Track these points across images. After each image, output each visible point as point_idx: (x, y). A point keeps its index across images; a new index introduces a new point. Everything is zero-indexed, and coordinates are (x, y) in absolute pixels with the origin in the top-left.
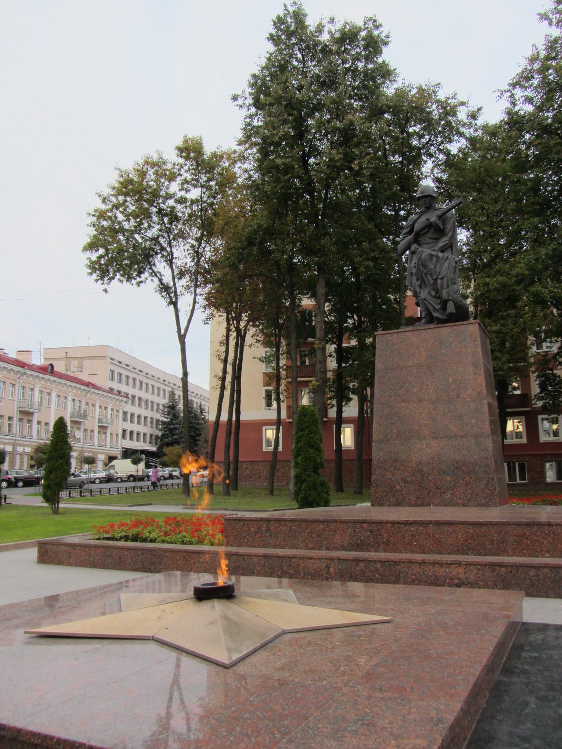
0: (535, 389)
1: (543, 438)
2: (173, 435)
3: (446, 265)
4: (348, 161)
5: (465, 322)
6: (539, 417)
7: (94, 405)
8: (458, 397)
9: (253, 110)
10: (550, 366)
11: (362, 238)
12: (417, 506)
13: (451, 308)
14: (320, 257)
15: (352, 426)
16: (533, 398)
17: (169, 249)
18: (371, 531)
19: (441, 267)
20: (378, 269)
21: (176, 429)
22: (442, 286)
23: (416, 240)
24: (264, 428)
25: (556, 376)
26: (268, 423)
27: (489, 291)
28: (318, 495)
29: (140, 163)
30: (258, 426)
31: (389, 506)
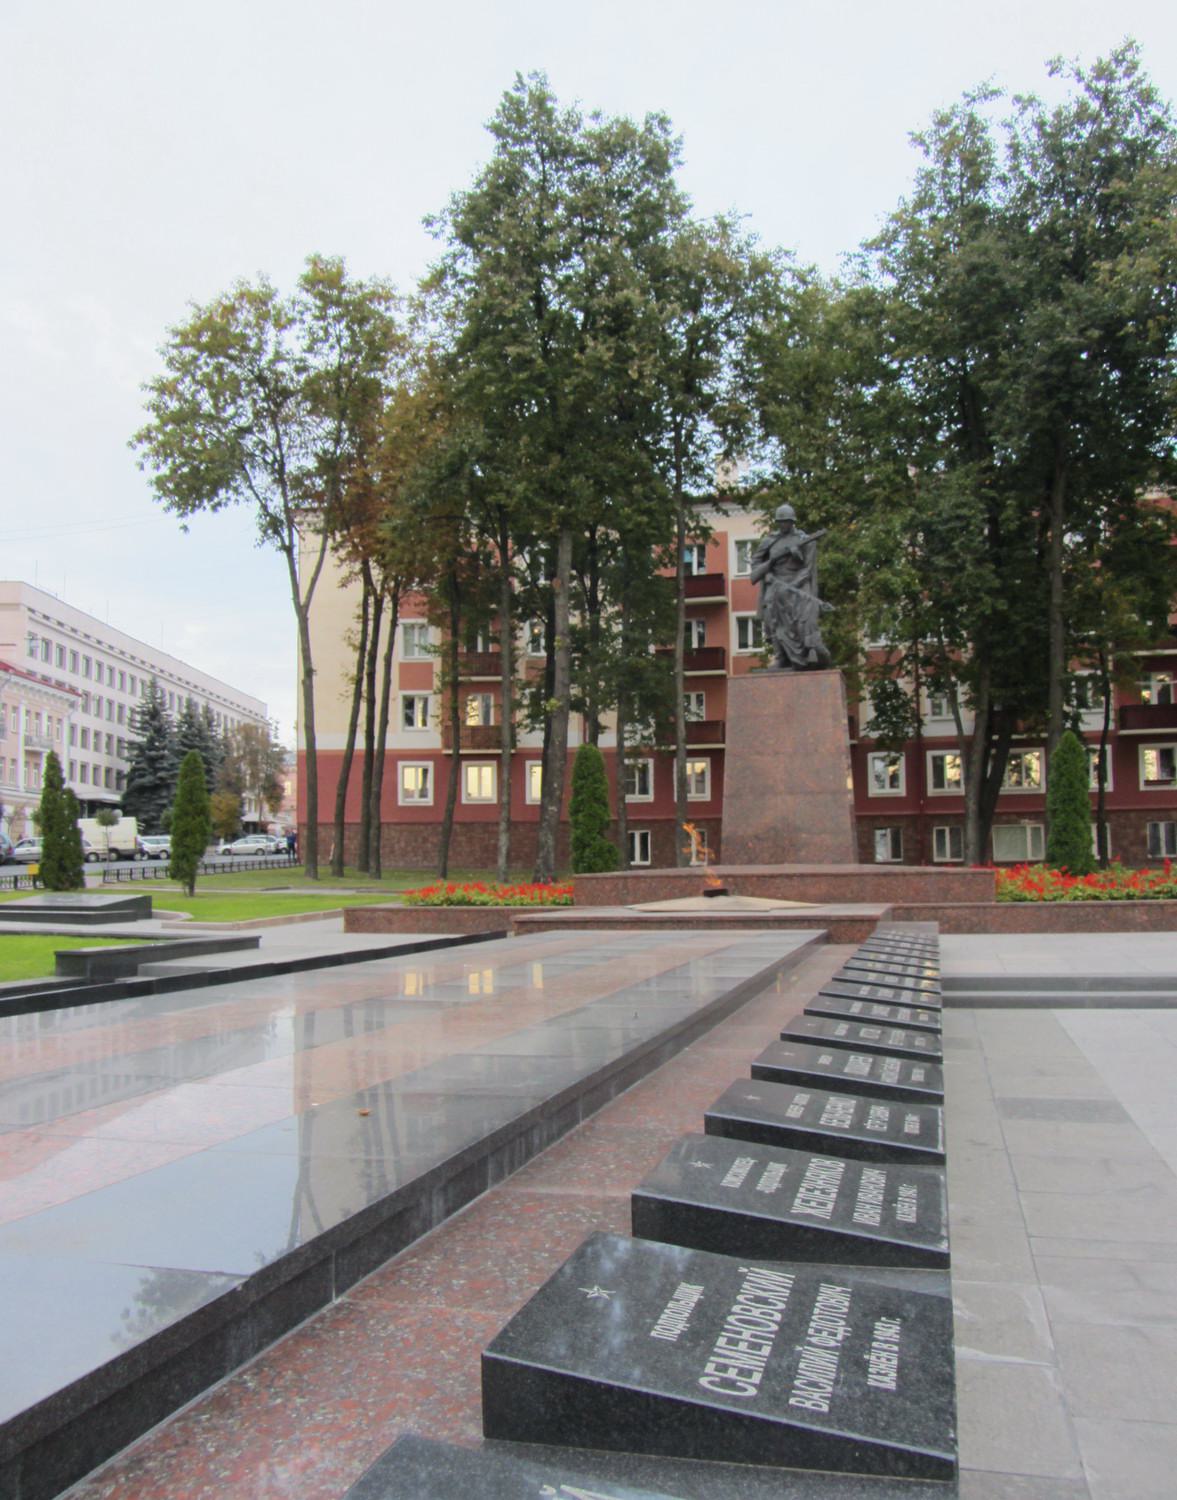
2: (157, 770)
3: (808, 607)
6: (870, 755)
7: (15, 709)
9: (457, 246)
14: (569, 506)
21: (163, 757)
23: (772, 569)
24: (401, 764)
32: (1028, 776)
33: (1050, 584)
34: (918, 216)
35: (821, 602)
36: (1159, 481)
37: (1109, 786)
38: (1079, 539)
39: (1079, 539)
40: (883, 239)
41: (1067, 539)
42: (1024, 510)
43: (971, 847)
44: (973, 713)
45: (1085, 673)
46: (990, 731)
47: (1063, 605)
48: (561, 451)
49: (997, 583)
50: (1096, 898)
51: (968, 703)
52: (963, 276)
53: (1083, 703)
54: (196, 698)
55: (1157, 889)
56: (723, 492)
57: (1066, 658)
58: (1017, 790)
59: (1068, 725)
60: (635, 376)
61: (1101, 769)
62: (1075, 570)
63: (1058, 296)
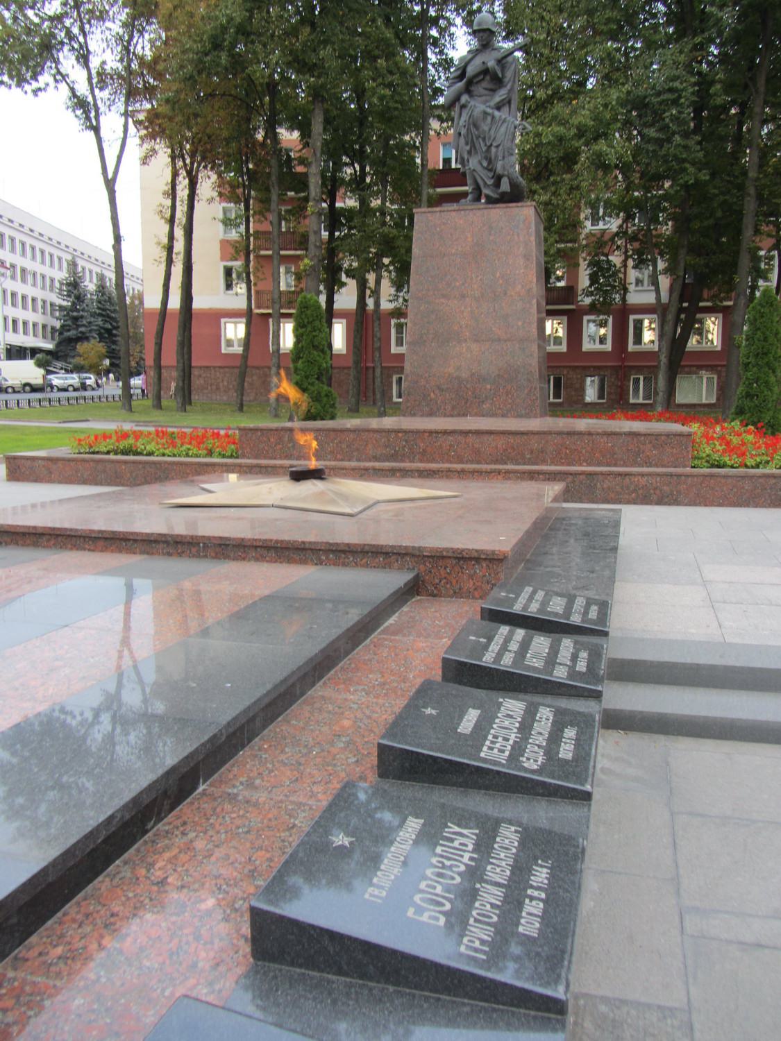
0: (584, 281)
1: (587, 346)
2: (78, 326)
3: (503, 129)
5: (520, 204)
6: (586, 318)
8: (505, 294)
10: (606, 251)
11: (377, 52)
12: (452, 416)
13: (505, 186)
14: (319, 77)
15: (344, 321)
16: (580, 293)
17: (81, 39)
18: (406, 441)
19: (497, 131)
20: (396, 102)
21: (82, 317)
22: (496, 156)
23: (468, 90)
24: (223, 320)
25: (610, 265)
26: (233, 314)
27: (540, 145)
30: (216, 317)
31: (422, 416)
43: (661, 394)
46: (682, 299)
47: (758, 179)
51: (666, 271)
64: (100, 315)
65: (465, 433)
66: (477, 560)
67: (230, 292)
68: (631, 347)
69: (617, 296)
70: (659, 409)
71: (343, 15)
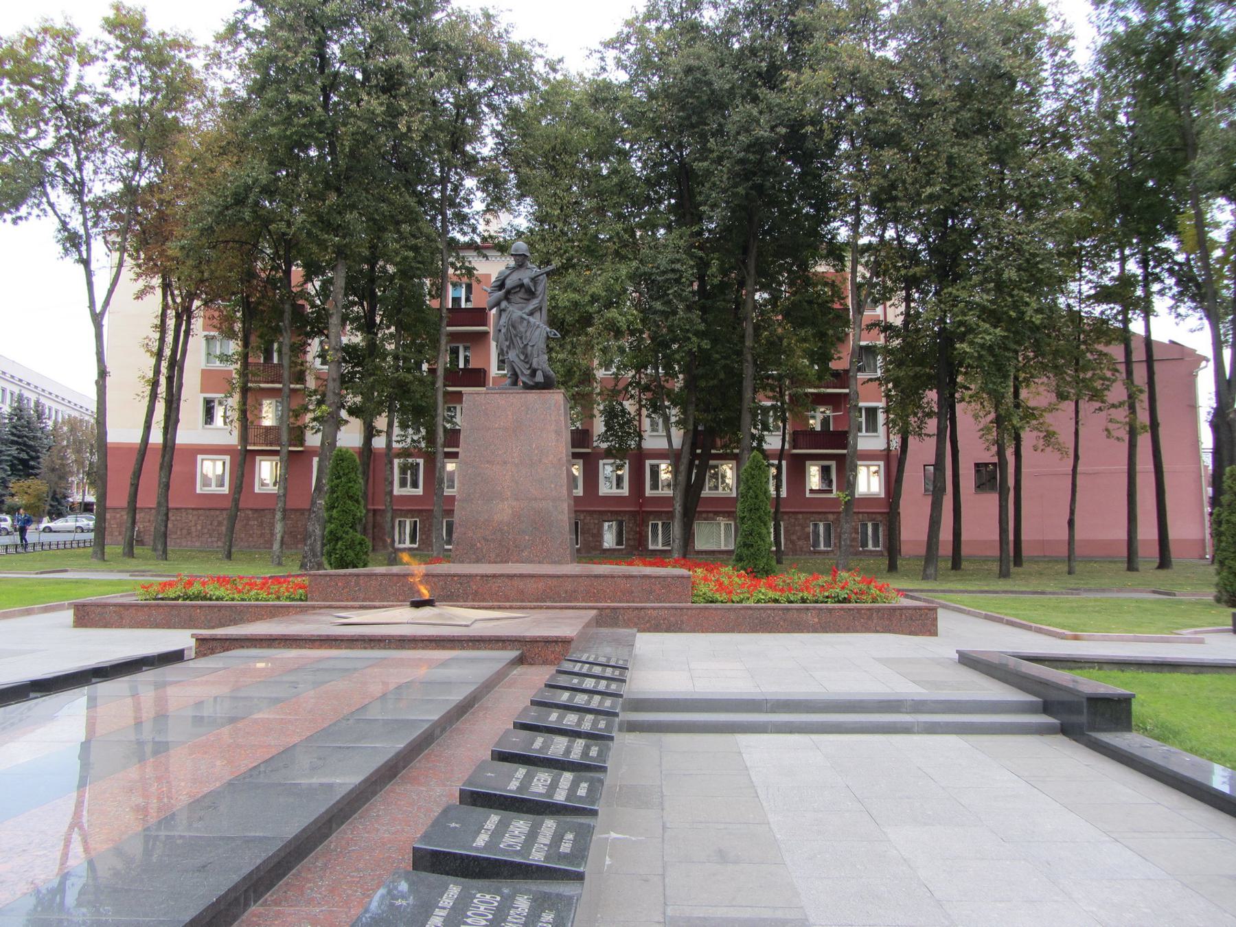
1: (605, 489)
3: (537, 333)
4: (391, 116)
6: (601, 462)
11: (401, 217)
12: (496, 563)
14: (344, 237)
16: (595, 439)
22: (532, 353)
23: (507, 297)
24: (200, 457)
28: (356, 555)
29: (32, 29)
32: (723, 482)
33: (744, 330)
34: (647, 25)
35: (548, 329)
36: (826, 257)
37: (784, 494)
38: (766, 296)
39: (766, 296)
40: (617, 40)
41: (757, 296)
42: (724, 272)
43: (677, 541)
44: (682, 431)
45: (769, 403)
46: (694, 446)
48: (338, 190)
49: (702, 327)
50: (776, 601)
51: (678, 423)
52: (681, 75)
53: (766, 427)
54: (26, 394)
55: (826, 594)
56: (484, 239)
57: (755, 391)
58: (713, 494)
59: (755, 444)
60: (404, 130)
61: (778, 477)
62: (762, 320)
63: (755, 99)
64: (13, 442)
65: (511, 577)
66: (556, 642)
67: (208, 426)
68: (648, 492)
69: (633, 442)
70: (676, 556)
71: (368, 184)
